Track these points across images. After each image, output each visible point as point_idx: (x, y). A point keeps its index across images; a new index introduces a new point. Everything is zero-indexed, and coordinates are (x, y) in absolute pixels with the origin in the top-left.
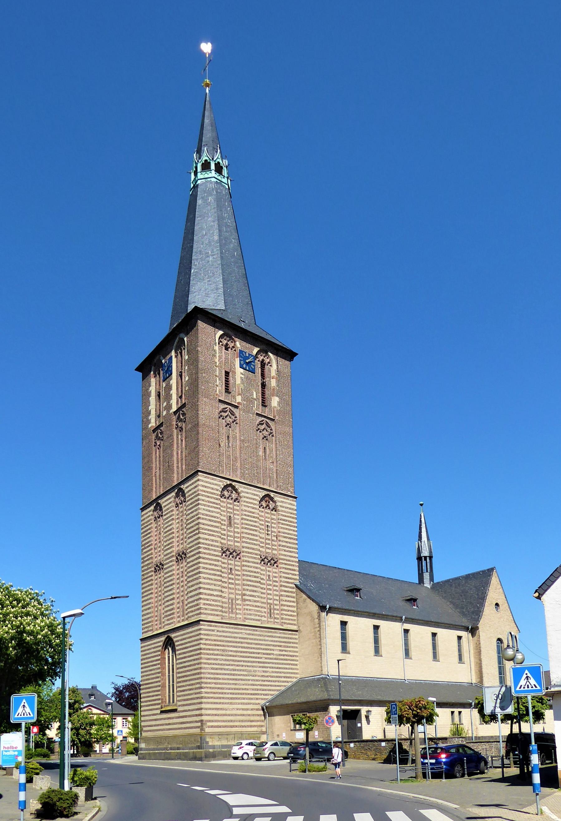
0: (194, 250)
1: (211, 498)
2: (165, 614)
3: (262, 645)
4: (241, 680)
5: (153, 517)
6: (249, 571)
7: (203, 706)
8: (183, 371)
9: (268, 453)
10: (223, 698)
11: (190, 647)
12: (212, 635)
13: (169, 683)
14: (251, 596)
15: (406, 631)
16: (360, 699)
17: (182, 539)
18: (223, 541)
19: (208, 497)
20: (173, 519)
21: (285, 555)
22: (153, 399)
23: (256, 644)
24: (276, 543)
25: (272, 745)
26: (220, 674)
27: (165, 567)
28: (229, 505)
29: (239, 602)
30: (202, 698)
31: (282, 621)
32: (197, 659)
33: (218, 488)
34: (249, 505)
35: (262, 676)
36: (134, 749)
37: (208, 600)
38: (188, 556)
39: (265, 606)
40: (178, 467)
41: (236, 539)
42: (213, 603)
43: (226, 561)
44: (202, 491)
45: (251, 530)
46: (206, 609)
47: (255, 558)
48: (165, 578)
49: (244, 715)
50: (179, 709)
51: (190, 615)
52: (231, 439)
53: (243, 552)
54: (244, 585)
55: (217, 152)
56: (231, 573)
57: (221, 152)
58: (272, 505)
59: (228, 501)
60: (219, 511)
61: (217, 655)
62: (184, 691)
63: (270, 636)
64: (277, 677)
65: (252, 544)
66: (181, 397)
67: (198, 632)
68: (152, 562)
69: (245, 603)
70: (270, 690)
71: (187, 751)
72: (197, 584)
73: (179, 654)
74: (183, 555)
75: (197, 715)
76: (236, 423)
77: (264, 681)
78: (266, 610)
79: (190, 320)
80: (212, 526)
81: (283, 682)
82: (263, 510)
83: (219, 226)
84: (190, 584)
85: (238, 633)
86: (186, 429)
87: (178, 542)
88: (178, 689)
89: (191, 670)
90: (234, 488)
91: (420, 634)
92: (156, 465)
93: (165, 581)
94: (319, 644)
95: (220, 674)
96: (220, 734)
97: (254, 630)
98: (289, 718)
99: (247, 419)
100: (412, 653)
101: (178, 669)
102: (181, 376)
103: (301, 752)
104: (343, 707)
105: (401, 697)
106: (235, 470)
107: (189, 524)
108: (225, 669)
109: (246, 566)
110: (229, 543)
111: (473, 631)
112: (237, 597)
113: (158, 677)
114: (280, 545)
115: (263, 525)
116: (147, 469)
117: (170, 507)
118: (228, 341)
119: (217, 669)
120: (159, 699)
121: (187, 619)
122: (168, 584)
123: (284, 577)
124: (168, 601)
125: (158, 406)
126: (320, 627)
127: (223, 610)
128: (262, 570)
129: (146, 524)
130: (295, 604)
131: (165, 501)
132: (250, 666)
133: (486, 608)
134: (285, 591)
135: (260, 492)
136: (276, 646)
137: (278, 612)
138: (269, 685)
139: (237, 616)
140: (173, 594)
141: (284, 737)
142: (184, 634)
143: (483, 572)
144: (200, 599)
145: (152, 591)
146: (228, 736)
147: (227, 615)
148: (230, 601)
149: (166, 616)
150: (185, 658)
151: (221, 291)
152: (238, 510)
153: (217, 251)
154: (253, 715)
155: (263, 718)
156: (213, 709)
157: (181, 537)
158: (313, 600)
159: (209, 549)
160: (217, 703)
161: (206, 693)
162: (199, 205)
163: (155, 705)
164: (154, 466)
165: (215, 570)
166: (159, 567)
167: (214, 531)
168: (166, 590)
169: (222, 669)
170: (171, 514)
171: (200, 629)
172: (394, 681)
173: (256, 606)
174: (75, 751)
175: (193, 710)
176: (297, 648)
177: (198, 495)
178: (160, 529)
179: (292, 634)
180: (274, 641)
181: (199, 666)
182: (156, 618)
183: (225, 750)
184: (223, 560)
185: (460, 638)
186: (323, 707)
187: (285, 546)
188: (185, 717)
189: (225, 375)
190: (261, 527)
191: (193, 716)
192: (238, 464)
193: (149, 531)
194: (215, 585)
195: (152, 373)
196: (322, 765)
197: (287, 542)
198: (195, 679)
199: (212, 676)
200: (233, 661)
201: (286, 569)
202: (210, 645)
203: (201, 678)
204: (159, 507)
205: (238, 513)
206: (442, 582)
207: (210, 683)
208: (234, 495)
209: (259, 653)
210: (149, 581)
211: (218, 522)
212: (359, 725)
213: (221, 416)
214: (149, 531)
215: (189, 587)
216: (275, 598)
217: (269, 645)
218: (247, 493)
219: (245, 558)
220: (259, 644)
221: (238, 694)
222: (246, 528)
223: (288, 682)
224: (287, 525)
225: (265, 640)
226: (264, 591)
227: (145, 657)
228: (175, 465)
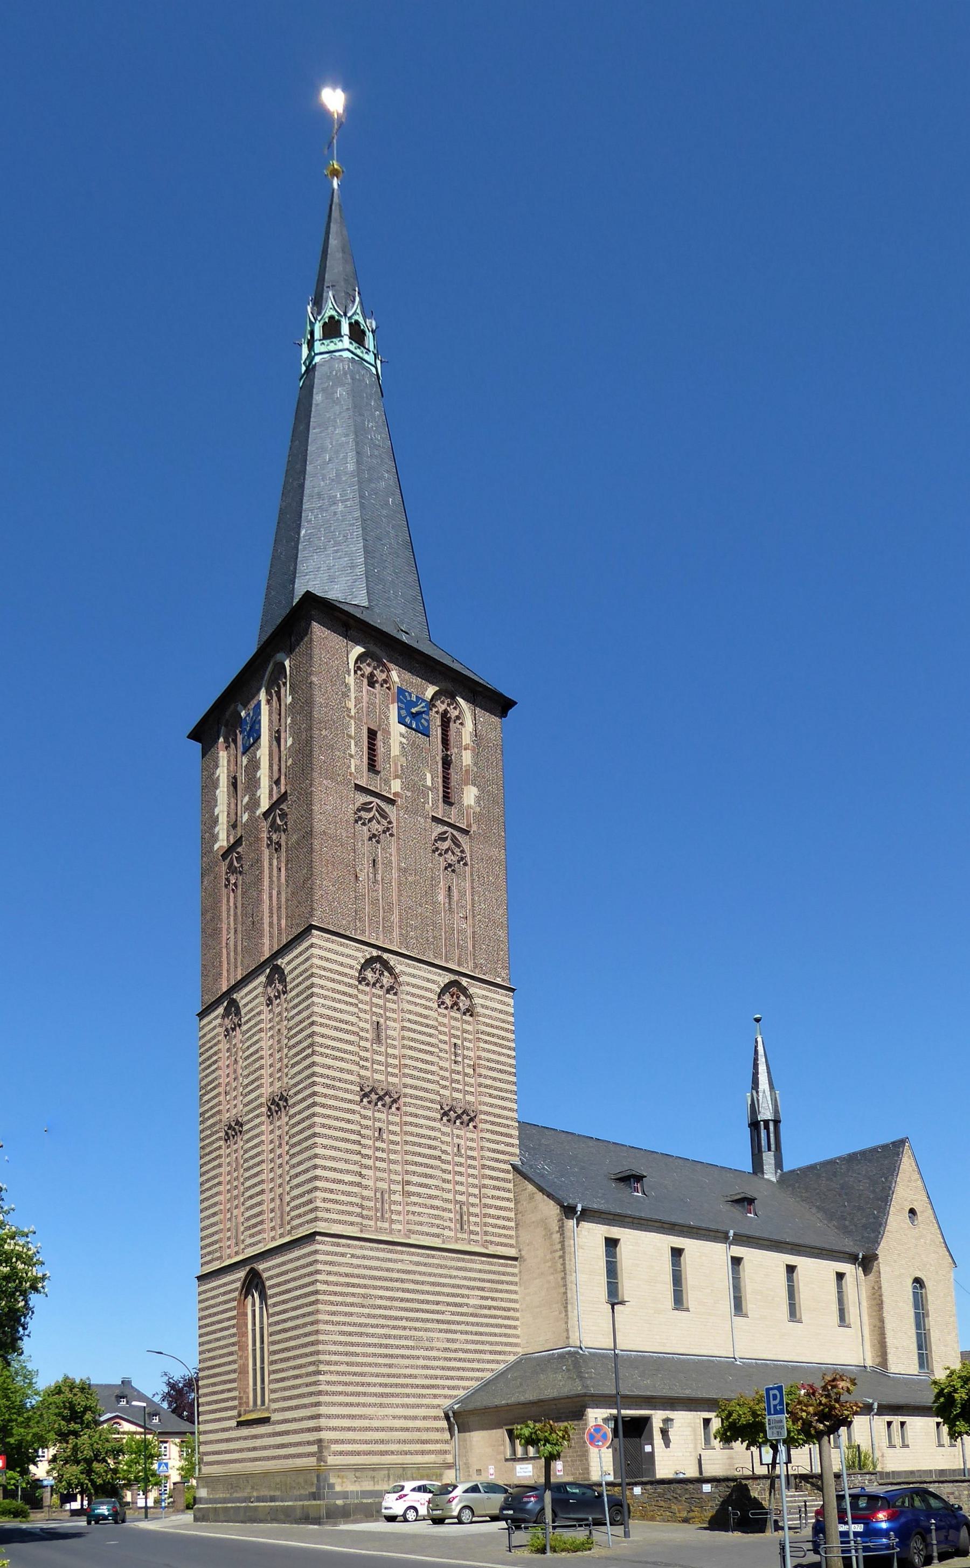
0: (307, 492)
1: (339, 982)
2: (245, 1225)
3: (444, 1285)
4: (403, 1357)
5: (222, 1030)
6: (418, 1135)
7: (323, 1410)
8: (282, 729)
9: (455, 898)
10: (365, 1394)
12: (340, 1264)
14: (421, 1185)
15: (736, 1261)
16: (649, 1393)
17: (280, 1070)
18: (363, 1072)
19: (333, 980)
20: (261, 1030)
21: (492, 1105)
23: (433, 1284)
24: (472, 1081)
25: (466, 1491)
26: (358, 1345)
27: (245, 1128)
28: (375, 1000)
30: (320, 1393)
31: (485, 1238)
32: (310, 1314)
33: (353, 963)
34: (418, 1001)
35: (446, 1350)
37: (331, 1191)
38: (291, 1102)
39: (451, 1206)
40: (271, 924)
41: (389, 1069)
43: (369, 1113)
44: (319, 967)
45: (421, 1051)
46: (328, 1210)
47: (429, 1109)
48: (246, 1152)
49: (407, 1429)
50: (275, 1417)
51: (295, 1223)
52: (380, 866)
53: (405, 1096)
54: (407, 1163)
55: (354, 302)
56: (380, 1138)
57: (361, 303)
58: (464, 1003)
59: (374, 991)
60: (356, 1010)
61: (352, 1305)
62: (283, 1380)
64: (476, 1351)
65: (424, 1079)
66: (277, 782)
67: (311, 1259)
68: (221, 1121)
69: (409, 1200)
70: (461, 1378)
72: (310, 1158)
73: (275, 1305)
74: (281, 1103)
75: (309, 1430)
76: (391, 835)
77: (450, 1359)
78: (452, 1215)
79: (297, 620)
80: (341, 1040)
81: (489, 1362)
82: (446, 1012)
83: (357, 444)
84: (294, 1161)
85: (396, 1261)
86: (287, 844)
87: (271, 1075)
88: (272, 1377)
89: (298, 1337)
90: (385, 964)
91: (764, 1266)
92: (229, 924)
93: (246, 1156)
94: (561, 1283)
95: (358, 1345)
97: (428, 1256)
98: (501, 1434)
99: (413, 827)
100: (750, 1304)
101: (271, 1335)
102: (278, 740)
103: (530, 1506)
104: (623, 1412)
105: (732, 1391)
106: (388, 930)
107: (292, 1037)
108: (367, 1335)
109: (411, 1124)
110: (377, 1076)
111: (867, 1263)
112: (393, 1187)
113: (231, 1354)
114: (480, 1085)
115: (445, 1043)
116: (210, 933)
117: (256, 1007)
118: (375, 668)
119: (350, 1334)
120: (233, 1399)
121: (289, 1232)
122: (251, 1163)
123: (489, 1150)
124: (251, 1197)
125: (233, 806)
126: (563, 1248)
127: (365, 1212)
128: (444, 1134)
129: (209, 1045)
130: (512, 1205)
131: (246, 995)
132: (420, 1330)
133: (891, 1218)
134: (492, 1178)
135: (440, 975)
136: (473, 1288)
137: (478, 1220)
138: (458, 1369)
139: (394, 1226)
140: (262, 1182)
141: (492, 1474)
142: (283, 1264)
143: (885, 1147)
144: (316, 1188)
145: (221, 1179)
147: (372, 1223)
148: (378, 1195)
149: (249, 1228)
150: (285, 1311)
151: (360, 570)
152: (394, 1011)
153: (352, 492)
155: (447, 1435)
156: (343, 1417)
157: (278, 1066)
158: (549, 1196)
159: (333, 1087)
160: (351, 1405)
161: (328, 1383)
162: (317, 405)
163: (226, 1409)
164: (225, 926)
165: (347, 1131)
166: (234, 1129)
167: (345, 1051)
168: (247, 1174)
169: (361, 1334)
170: (258, 1019)
171: (316, 1252)
172: (713, 1361)
173: (432, 1207)
175: (302, 1419)
176: (516, 1292)
177: (312, 975)
178: (236, 1052)
179: (506, 1265)
180: (470, 1279)
181: (314, 1328)
182: (229, 1234)
183: (369, 1501)
184: (364, 1112)
185: (840, 1276)
186: (574, 1409)
187: (490, 1087)
188: (287, 1433)
189: (369, 737)
190: (442, 1046)
192: (395, 918)
193: (215, 1058)
194: (346, 1161)
195: (221, 740)
196: (580, 1535)
197: (494, 1079)
198: (306, 1355)
199: (341, 1349)
200: (385, 1317)
201: (492, 1132)
202: (337, 1284)
203: (318, 1353)
204: (233, 1008)
205: (395, 1016)
206: (799, 1169)
207: (336, 1363)
208: (386, 980)
209: (438, 1303)
210: (214, 1159)
211: (354, 1033)
212: (648, 1448)
213: (360, 818)
214: (215, 1058)
215: (293, 1166)
216: (472, 1190)
217: (459, 1287)
218: (414, 976)
219: (408, 1109)
220: (439, 1284)
221: (396, 1385)
222: (411, 1048)
223: (498, 1362)
224: (495, 1044)
225: (451, 1277)
226: (449, 1177)
227: (206, 1313)
228: (266, 920)
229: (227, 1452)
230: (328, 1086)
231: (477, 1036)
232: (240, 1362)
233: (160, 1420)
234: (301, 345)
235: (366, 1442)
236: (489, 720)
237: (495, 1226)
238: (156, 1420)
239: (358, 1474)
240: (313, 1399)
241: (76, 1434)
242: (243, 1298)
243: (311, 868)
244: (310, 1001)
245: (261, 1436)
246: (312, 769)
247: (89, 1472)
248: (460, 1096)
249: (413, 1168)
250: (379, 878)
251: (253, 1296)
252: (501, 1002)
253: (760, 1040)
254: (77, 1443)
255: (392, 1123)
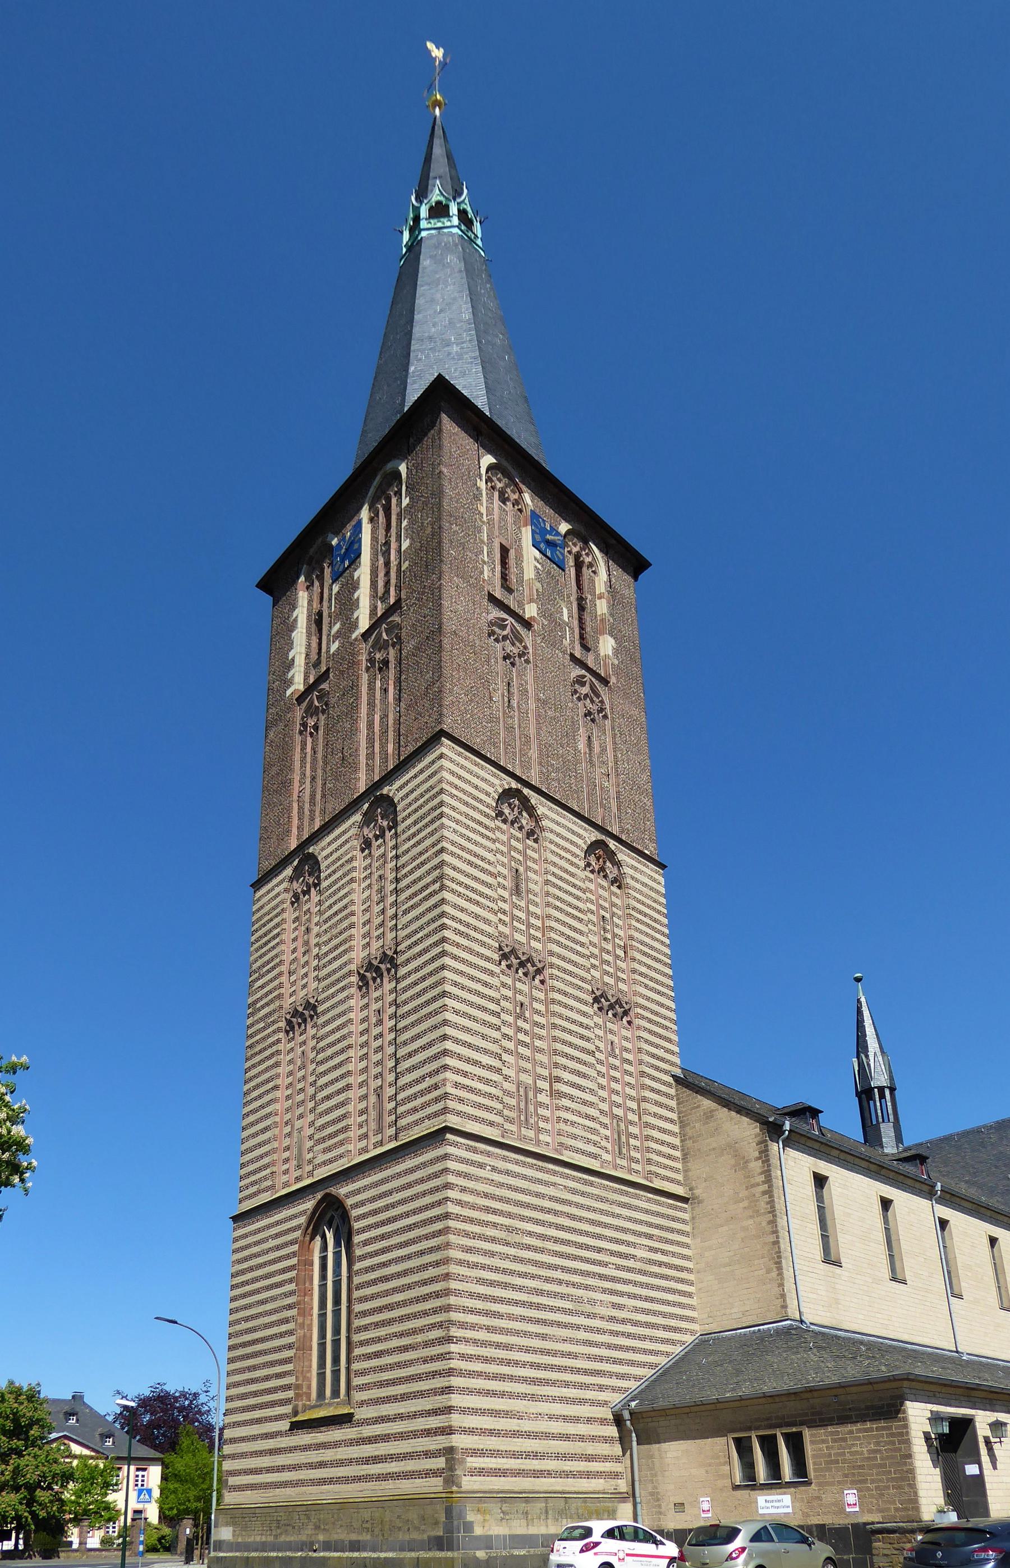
1: (474, 808)
3: (606, 1226)
4: (559, 1324)
5: (288, 896)
10: (511, 1378)
11: (407, 1214)
12: (477, 1179)
13: (322, 1335)
14: (574, 1085)
20: (352, 880)
22: (300, 636)
23: (593, 1222)
29: (543, 1098)
33: (490, 790)
34: (563, 854)
35: (612, 1319)
36: (159, 1540)
37: (465, 1074)
42: (480, 1086)
46: (461, 1100)
47: (580, 988)
53: (552, 966)
56: (520, 1016)
61: (493, 1240)
62: (378, 1355)
63: (624, 1205)
65: (572, 950)
68: (281, 1007)
70: (632, 1363)
71: (390, 1555)
75: (428, 1433)
78: (608, 1133)
80: (476, 879)
85: (547, 1184)
90: (525, 801)
96: (506, 1498)
97: (586, 1183)
109: (560, 1003)
110: (517, 936)
113: (286, 1321)
119: (492, 1284)
123: (648, 1053)
134: (653, 1090)
137: (638, 1143)
139: (542, 1137)
145: (279, 1082)
146: (529, 1507)
148: (522, 1090)
154: (593, 1439)
155: (617, 1449)
159: (467, 936)
161: (463, 1357)
163: (272, 1404)
167: (481, 894)
169: (505, 1286)
171: (446, 1157)
174: (21, 1542)
175: (414, 1415)
176: (687, 1246)
183: (523, 1552)
188: (385, 1438)
191: (415, 1434)
193: (275, 932)
195: (302, 579)
198: (425, 1313)
199: (479, 1305)
200: (536, 1263)
201: (650, 1032)
202: (473, 1207)
203: (448, 1308)
207: (473, 1327)
208: (525, 820)
214: (275, 932)
220: (599, 1224)
222: (557, 908)
223: (673, 1342)
228: (363, 752)
229: (269, 1470)
230: (461, 933)
231: (628, 911)
232: (300, 1332)
233: (114, 1443)
234: (402, 233)
235: (515, 1455)
236: (622, 578)
237: (659, 1153)
238: (109, 1443)
239: (505, 1507)
240: (438, 1383)
241: (20, 1454)
242: (308, 1238)
243: (439, 667)
244: (438, 823)
245: (336, 1444)
246: (441, 561)
247: (30, 1502)
248: (611, 981)
249: (563, 1061)
250: (514, 703)
251: (324, 1237)
252: (651, 878)
253: (863, 1000)
254: (19, 1465)
255: (536, 1000)
